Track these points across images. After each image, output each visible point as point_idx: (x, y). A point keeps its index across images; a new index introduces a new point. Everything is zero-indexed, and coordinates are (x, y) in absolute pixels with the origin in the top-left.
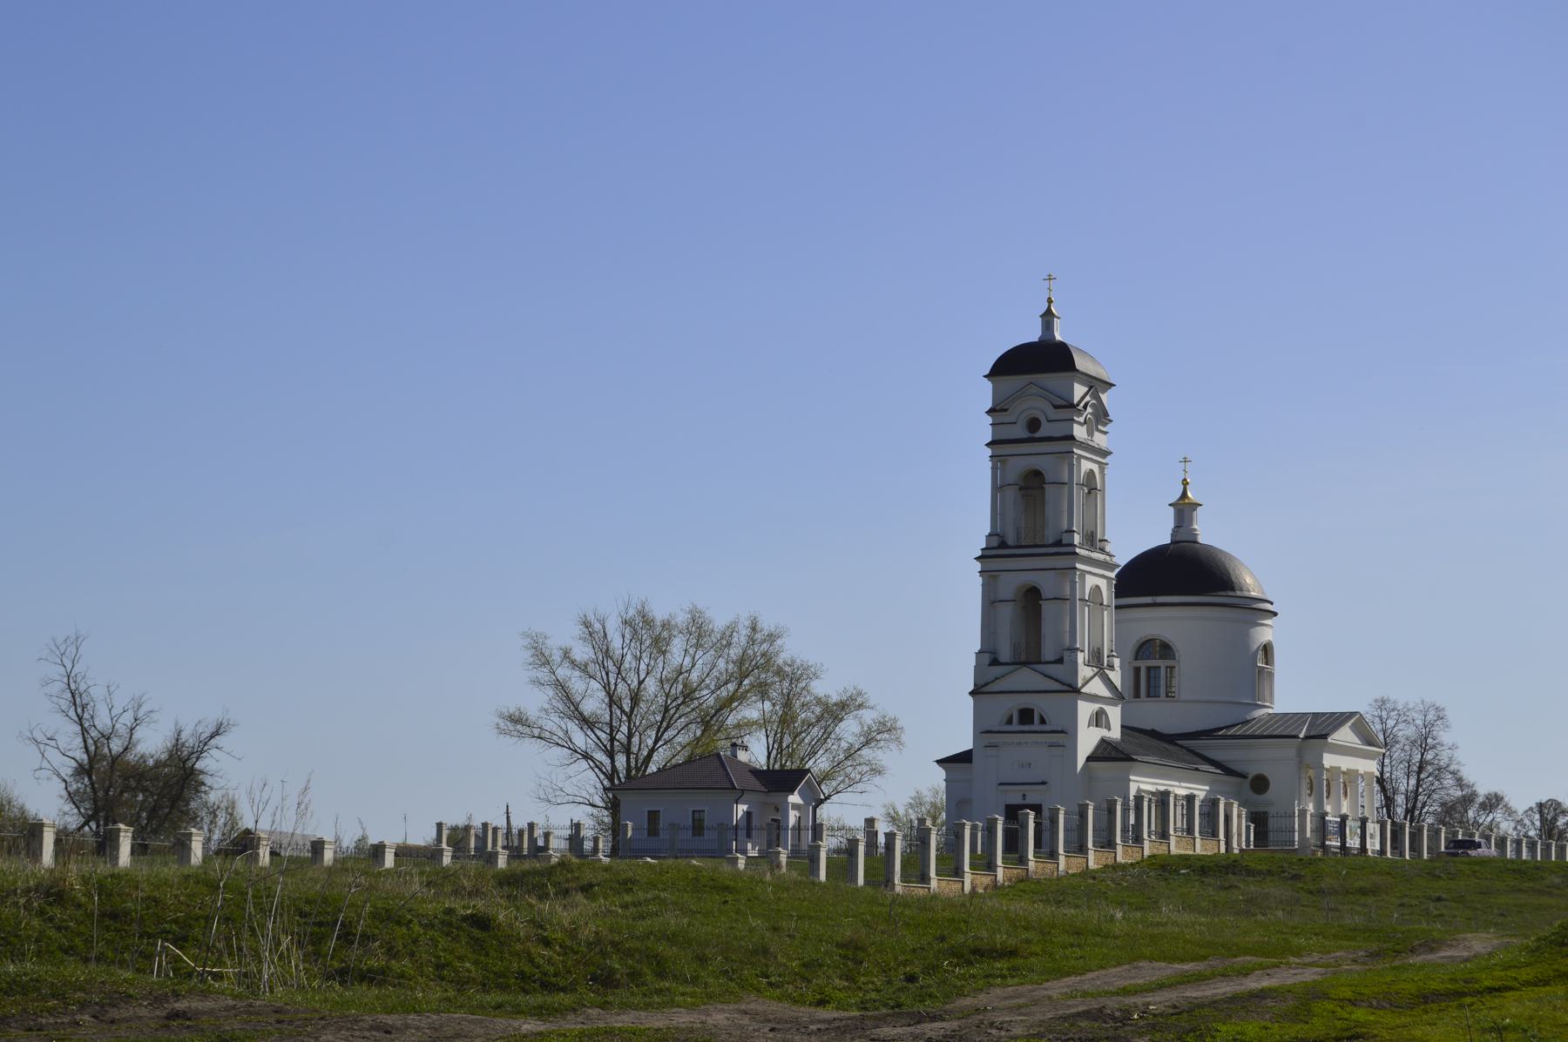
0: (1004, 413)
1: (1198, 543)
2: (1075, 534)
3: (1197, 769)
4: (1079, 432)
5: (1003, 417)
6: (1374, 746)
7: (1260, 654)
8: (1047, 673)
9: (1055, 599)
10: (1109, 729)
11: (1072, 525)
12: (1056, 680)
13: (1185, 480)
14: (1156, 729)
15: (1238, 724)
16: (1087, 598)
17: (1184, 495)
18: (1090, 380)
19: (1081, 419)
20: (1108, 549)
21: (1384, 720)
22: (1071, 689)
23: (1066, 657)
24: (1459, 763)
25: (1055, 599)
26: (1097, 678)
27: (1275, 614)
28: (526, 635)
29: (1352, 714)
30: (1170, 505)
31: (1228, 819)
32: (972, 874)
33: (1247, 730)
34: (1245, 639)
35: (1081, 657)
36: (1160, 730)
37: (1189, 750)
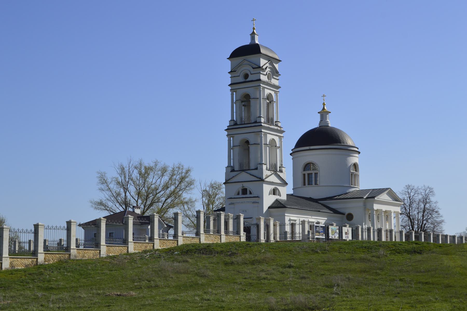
0: (235, 72)
1: (328, 126)
2: (262, 118)
3: (319, 211)
4: (264, 78)
5: (235, 74)
7: (352, 168)
8: (251, 174)
9: (254, 144)
10: (280, 196)
11: (261, 115)
12: (255, 176)
13: (324, 103)
14: (311, 197)
15: (343, 194)
16: (268, 144)
17: (324, 109)
18: (269, 58)
19: (265, 73)
20: (279, 125)
21: (410, 193)
22: (260, 180)
23: (258, 167)
24: (439, 208)
25: (254, 144)
26: (273, 175)
27: (359, 153)
28: (98, 173)
29: (387, 189)
30: (318, 113)
31: (267, 227)
32: (10, 258)
33: (341, 197)
34: (345, 162)
35: (264, 167)
36: (312, 198)
37: (322, 205)
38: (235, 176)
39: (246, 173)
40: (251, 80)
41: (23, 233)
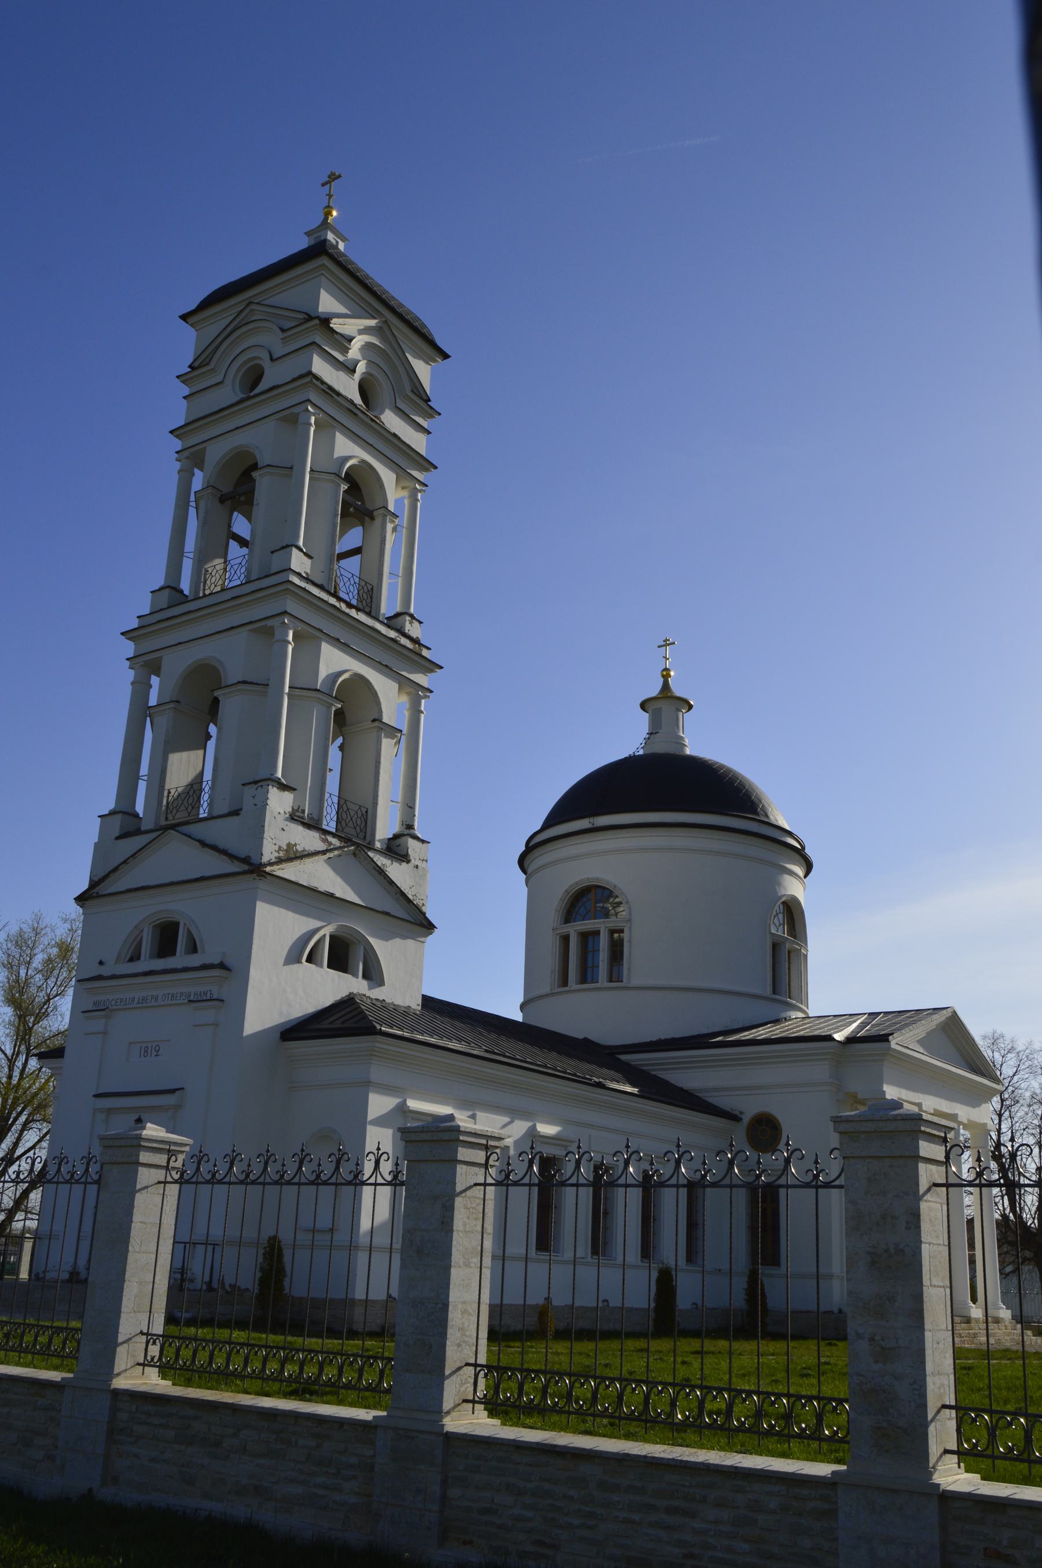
6: (982, 1074)
8: (209, 841)
10: (381, 983)
12: (223, 852)
17: (666, 687)
35: (279, 803)
36: (595, 1041)
38: (132, 856)
39: (223, 852)
40: (271, 386)
41: (86, 1183)
